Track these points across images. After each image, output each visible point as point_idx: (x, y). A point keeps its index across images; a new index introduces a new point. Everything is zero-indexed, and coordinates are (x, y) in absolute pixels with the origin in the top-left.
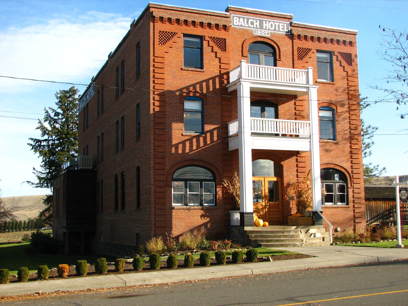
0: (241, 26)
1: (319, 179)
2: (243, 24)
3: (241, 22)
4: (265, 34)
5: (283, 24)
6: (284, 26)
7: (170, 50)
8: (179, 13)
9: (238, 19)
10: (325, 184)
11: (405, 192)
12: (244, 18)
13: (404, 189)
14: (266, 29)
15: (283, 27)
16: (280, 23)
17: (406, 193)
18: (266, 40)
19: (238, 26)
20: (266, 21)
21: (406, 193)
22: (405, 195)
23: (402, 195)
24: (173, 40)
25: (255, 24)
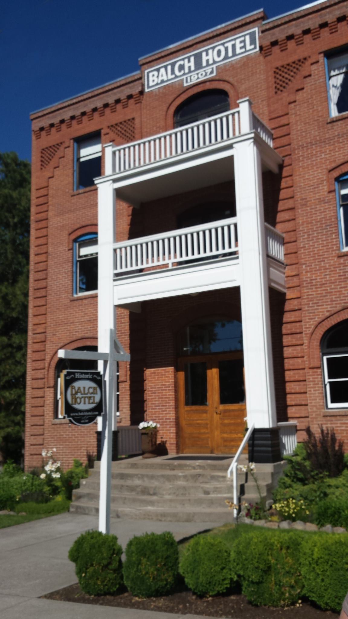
0: (163, 81)
1: (54, 369)
2: (165, 78)
3: (162, 76)
4: (206, 75)
5: (242, 39)
6: (244, 41)
7: (57, 172)
8: (262, 118)
9: (156, 73)
10: (333, 401)
11: (93, 385)
12: (166, 67)
13: (87, 376)
14: (208, 65)
15: (242, 44)
16: (235, 39)
17: (95, 389)
18: (208, 86)
19: (157, 84)
20: (207, 51)
21: (95, 389)
22: (90, 398)
23: (79, 395)
24: (59, 153)
25: (187, 66)
